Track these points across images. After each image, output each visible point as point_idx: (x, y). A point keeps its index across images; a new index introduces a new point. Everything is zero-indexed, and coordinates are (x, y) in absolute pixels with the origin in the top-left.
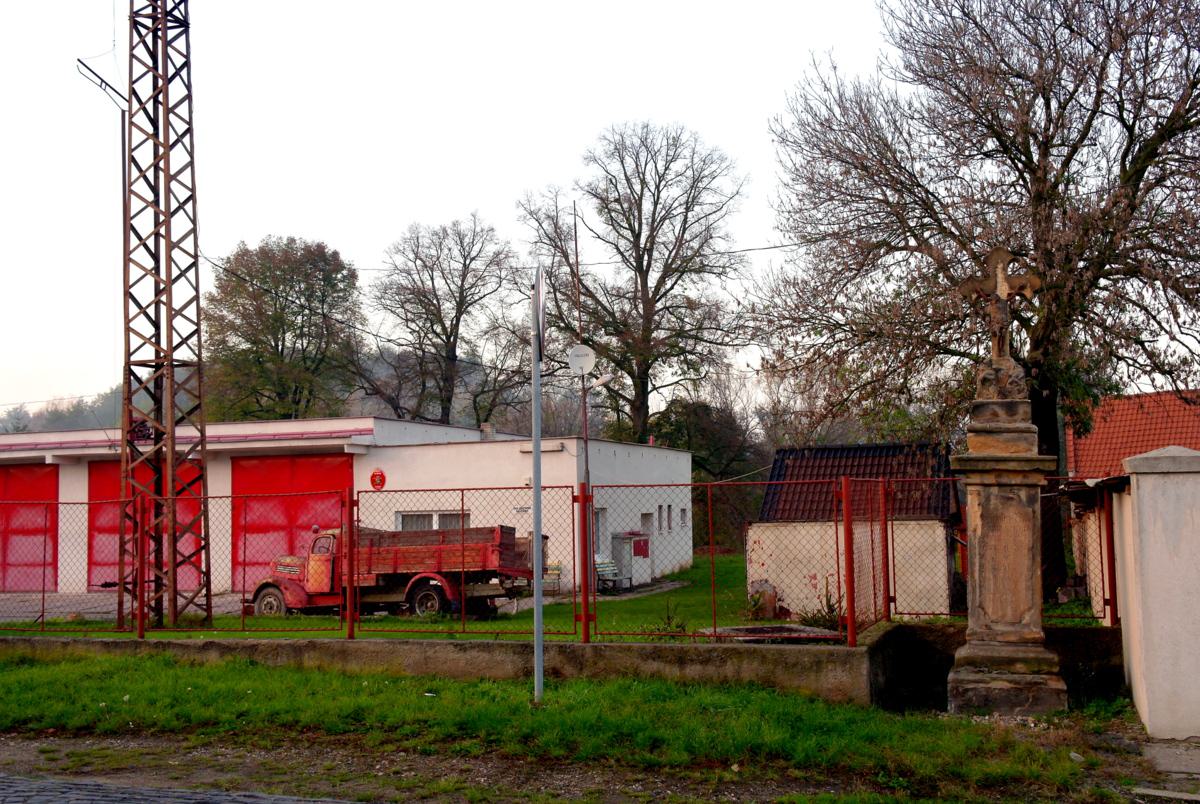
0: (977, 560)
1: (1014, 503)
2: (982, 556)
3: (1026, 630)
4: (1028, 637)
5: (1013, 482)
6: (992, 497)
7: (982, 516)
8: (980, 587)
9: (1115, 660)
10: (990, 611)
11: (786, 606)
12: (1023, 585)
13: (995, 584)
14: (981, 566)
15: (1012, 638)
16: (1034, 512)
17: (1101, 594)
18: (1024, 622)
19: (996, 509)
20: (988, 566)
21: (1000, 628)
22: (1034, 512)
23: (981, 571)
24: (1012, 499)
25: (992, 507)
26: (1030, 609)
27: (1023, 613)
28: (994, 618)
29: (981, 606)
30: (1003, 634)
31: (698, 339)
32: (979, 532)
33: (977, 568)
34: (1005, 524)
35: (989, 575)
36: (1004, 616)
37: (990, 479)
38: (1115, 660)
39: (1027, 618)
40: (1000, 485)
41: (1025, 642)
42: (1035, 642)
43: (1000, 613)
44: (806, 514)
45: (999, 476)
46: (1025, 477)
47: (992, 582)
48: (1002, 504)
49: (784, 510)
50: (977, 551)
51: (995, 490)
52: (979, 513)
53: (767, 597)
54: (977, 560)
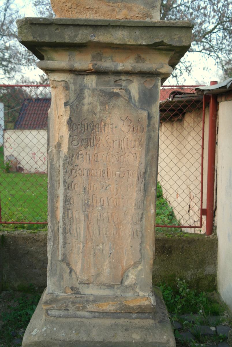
0: (61, 192)
1: (121, 102)
2: (68, 186)
3: (130, 294)
4: (132, 304)
5: (120, 67)
6: (87, 93)
7: (70, 122)
8: (65, 232)
9: (208, 270)
10: (78, 268)
11: (21, 166)
12: (127, 230)
13: (87, 227)
14: (67, 201)
15: (109, 307)
16: (150, 117)
17: (199, 204)
18: (127, 283)
19: (92, 112)
20: (77, 201)
21: (91, 291)
22: (150, 117)
23: (66, 210)
24: (117, 95)
25: (86, 108)
27: (127, 270)
28: (84, 278)
29: (65, 260)
30: (96, 300)
31: (10, 62)
32: (65, 149)
33: (60, 204)
34: (104, 137)
35: (78, 214)
36: (98, 275)
37: (83, 61)
38: (208, 270)
39: (131, 278)
40: (98, 72)
41: (126, 312)
42: (141, 311)
43: (93, 271)
44: (32, 126)
45: (98, 57)
46: (139, 59)
47: (82, 225)
48: (102, 104)
49: (25, 124)
50: (62, 182)
51: (91, 81)
52: (66, 118)
53: (13, 163)
54: (61, 192)
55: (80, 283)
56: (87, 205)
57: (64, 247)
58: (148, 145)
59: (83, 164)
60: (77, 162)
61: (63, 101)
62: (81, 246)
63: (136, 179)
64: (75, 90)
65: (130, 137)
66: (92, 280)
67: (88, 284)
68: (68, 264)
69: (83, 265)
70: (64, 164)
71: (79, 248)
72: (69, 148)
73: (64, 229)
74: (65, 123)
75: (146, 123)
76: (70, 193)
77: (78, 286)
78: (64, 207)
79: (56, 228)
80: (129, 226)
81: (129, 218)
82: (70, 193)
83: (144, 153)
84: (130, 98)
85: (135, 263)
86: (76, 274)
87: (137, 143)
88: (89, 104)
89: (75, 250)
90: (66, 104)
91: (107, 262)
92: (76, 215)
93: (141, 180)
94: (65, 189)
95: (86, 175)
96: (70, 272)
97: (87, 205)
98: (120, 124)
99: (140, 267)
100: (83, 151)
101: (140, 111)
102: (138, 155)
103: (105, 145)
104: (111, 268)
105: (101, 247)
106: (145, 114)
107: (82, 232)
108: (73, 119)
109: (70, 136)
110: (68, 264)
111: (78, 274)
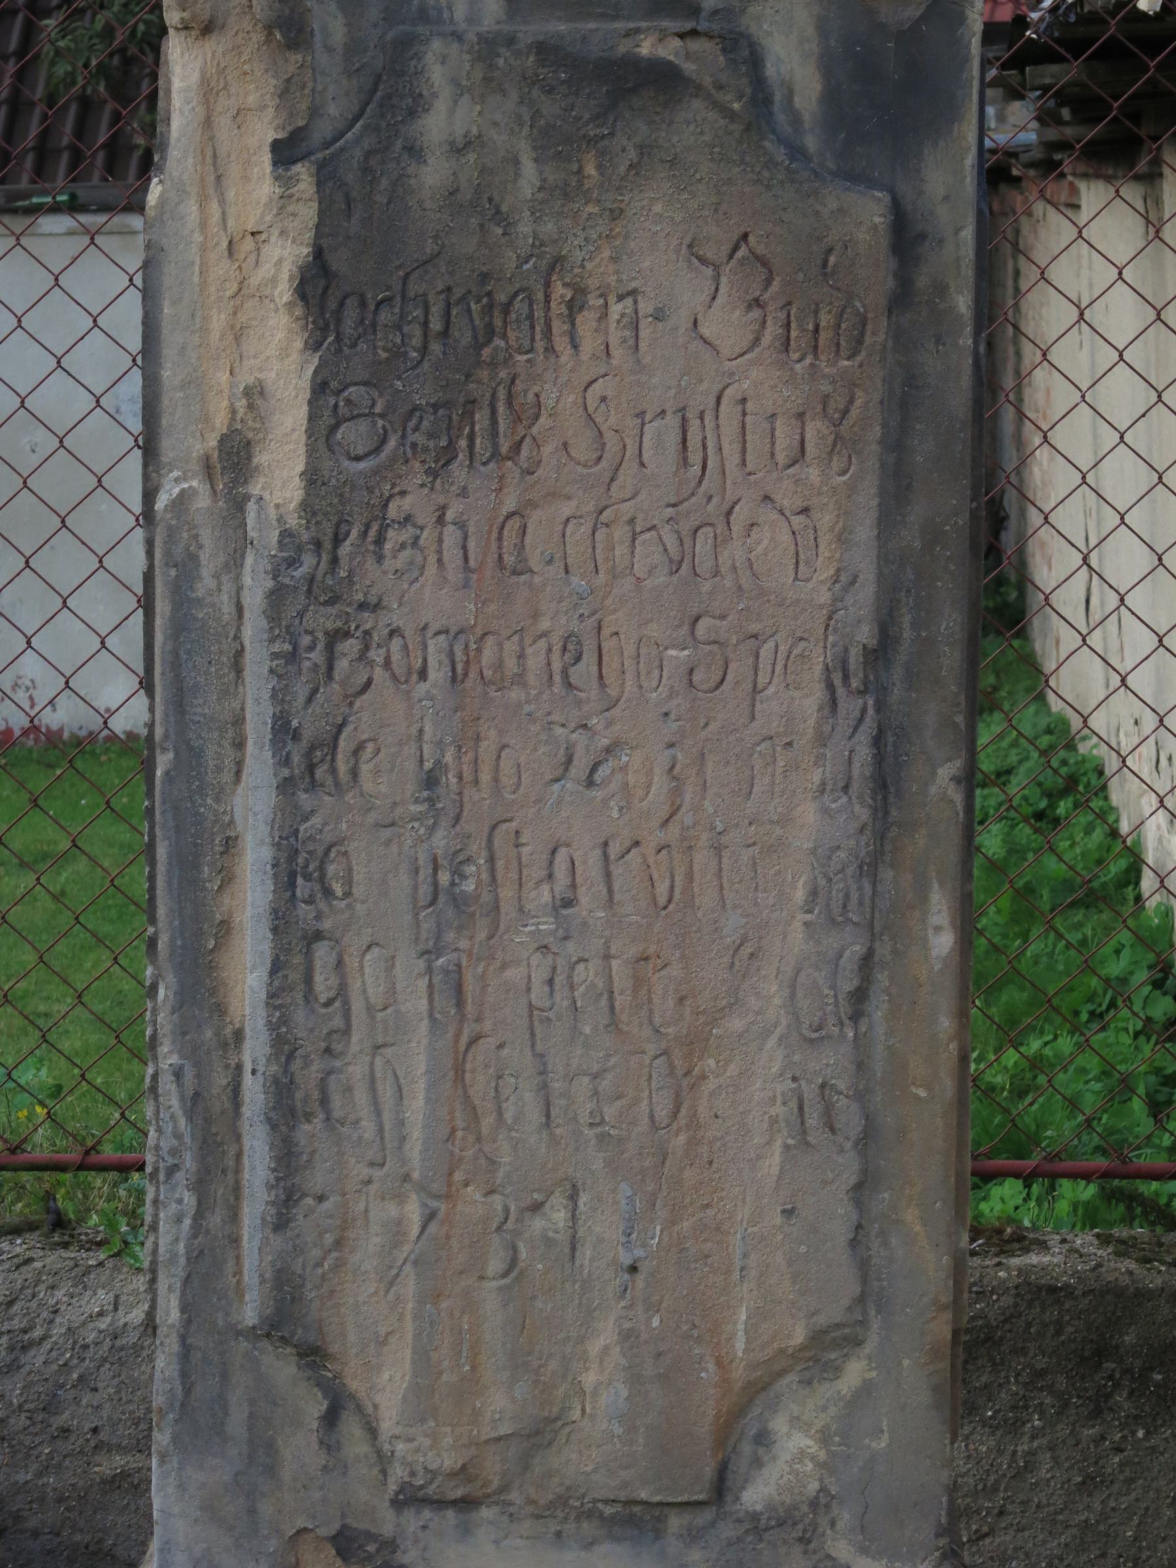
1: (693, 127)
2: (311, 760)
6: (440, 67)
7: (317, 286)
10: (387, 1387)
14: (301, 869)
18: (756, 1495)
19: (484, 206)
20: (377, 876)
24: (664, 80)
25: (433, 175)
26: (824, 1350)
27: (758, 1389)
29: (296, 1330)
32: (281, 479)
34: (574, 384)
35: (383, 972)
36: (540, 1434)
39: (791, 1456)
43: (501, 1405)
47: (417, 1057)
48: (556, 144)
52: (283, 257)
55: (409, 1499)
56: (451, 904)
57: (281, 1223)
58: (896, 446)
59: (420, 593)
60: (376, 578)
61: (265, 131)
62: (413, 1211)
63: (811, 702)
64: (353, 48)
65: (766, 385)
66: (493, 1468)
67: (467, 1504)
68: (313, 1356)
69: (423, 1357)
70: (276, 597)
71: (397, 1228)
72: (312, 478)
73: (282, 1091)
74: (284, 292)
75: (875, 280)
76: (324, 815)
77: (387, 1523)
78: (280, 921)
79: (221, 1080)
80: (772, 1058)
81: (769, 995)
82: (324, 815)
83: (867, 501)
84: (760, 95)
85: (819, 1339)
86: (372, 1432)
87: (815, 429)
88: (458, 149)
89: (367, 1251)
90: (285, 153)
91: (605, 1335)
92: (368, 980)
93: (849, 706)
94: (286, 787)
95: (437, 674)
96: (331, 1419)
97: (451, 904)
98: (689, 290)
99: (855, 1372)
100: (414, 501)
101: (833, 198)
102: (825, 519)
103: (582, 449)
104: (634, 1378)
105: (560, 1216)
106: (868, 214)
107: (416, 1107)
108: (338, 262)
109: (320, 388)
110: (313, 1356)
111: (387, 1426)
